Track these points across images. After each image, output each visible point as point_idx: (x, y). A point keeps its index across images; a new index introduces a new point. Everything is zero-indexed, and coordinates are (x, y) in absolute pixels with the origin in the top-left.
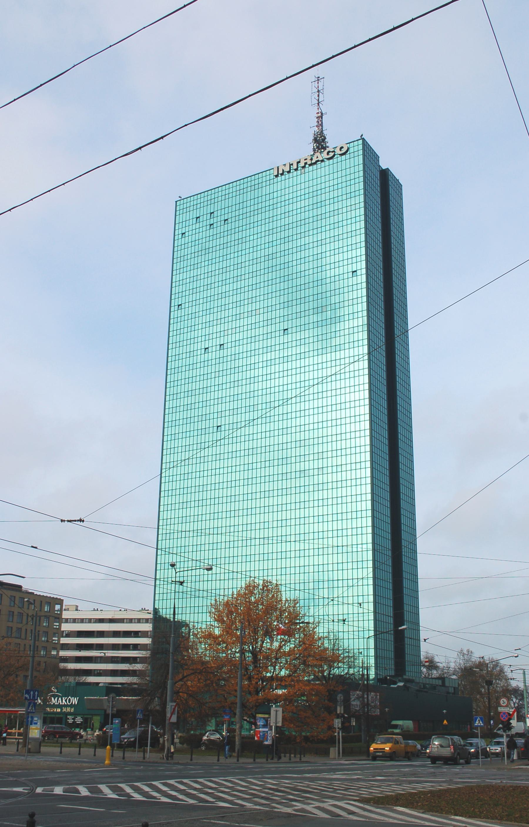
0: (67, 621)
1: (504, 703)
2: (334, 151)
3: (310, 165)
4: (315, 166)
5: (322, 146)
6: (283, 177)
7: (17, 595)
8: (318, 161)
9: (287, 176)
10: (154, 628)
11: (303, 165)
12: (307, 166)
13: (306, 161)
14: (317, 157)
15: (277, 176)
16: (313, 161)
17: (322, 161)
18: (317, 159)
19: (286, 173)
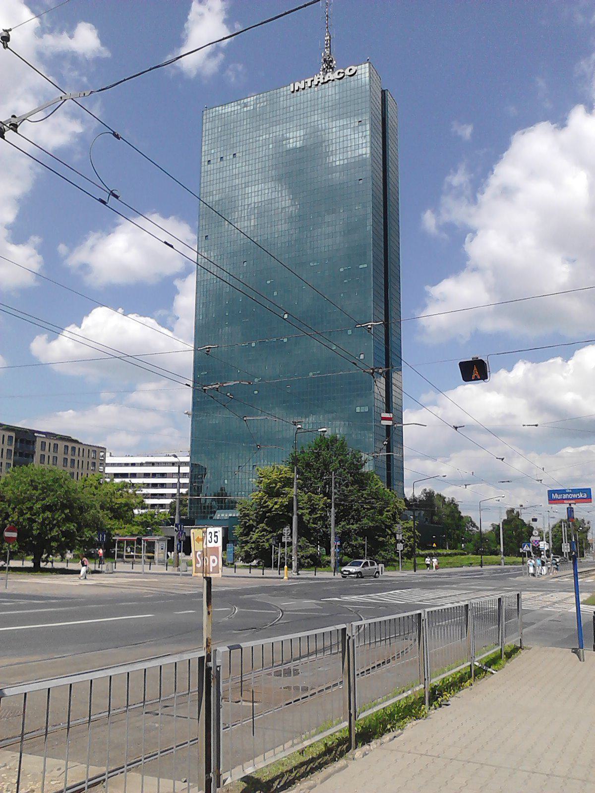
0: (108, 465)
1: (536, 533)
2: (344, 73)
4: (327, 84)
5: (330, 66)
6: (299, 93)
7: (77, 446)
8: (330, 80)
9: (302, 92)
10: (191, 471)
11: (317, 83)
12: (320, 84)
14: (329, 77)
15: (293, 92)
16: (326, 80)
17: (333, 80)
18: (329, 79)
19: (301, 90)
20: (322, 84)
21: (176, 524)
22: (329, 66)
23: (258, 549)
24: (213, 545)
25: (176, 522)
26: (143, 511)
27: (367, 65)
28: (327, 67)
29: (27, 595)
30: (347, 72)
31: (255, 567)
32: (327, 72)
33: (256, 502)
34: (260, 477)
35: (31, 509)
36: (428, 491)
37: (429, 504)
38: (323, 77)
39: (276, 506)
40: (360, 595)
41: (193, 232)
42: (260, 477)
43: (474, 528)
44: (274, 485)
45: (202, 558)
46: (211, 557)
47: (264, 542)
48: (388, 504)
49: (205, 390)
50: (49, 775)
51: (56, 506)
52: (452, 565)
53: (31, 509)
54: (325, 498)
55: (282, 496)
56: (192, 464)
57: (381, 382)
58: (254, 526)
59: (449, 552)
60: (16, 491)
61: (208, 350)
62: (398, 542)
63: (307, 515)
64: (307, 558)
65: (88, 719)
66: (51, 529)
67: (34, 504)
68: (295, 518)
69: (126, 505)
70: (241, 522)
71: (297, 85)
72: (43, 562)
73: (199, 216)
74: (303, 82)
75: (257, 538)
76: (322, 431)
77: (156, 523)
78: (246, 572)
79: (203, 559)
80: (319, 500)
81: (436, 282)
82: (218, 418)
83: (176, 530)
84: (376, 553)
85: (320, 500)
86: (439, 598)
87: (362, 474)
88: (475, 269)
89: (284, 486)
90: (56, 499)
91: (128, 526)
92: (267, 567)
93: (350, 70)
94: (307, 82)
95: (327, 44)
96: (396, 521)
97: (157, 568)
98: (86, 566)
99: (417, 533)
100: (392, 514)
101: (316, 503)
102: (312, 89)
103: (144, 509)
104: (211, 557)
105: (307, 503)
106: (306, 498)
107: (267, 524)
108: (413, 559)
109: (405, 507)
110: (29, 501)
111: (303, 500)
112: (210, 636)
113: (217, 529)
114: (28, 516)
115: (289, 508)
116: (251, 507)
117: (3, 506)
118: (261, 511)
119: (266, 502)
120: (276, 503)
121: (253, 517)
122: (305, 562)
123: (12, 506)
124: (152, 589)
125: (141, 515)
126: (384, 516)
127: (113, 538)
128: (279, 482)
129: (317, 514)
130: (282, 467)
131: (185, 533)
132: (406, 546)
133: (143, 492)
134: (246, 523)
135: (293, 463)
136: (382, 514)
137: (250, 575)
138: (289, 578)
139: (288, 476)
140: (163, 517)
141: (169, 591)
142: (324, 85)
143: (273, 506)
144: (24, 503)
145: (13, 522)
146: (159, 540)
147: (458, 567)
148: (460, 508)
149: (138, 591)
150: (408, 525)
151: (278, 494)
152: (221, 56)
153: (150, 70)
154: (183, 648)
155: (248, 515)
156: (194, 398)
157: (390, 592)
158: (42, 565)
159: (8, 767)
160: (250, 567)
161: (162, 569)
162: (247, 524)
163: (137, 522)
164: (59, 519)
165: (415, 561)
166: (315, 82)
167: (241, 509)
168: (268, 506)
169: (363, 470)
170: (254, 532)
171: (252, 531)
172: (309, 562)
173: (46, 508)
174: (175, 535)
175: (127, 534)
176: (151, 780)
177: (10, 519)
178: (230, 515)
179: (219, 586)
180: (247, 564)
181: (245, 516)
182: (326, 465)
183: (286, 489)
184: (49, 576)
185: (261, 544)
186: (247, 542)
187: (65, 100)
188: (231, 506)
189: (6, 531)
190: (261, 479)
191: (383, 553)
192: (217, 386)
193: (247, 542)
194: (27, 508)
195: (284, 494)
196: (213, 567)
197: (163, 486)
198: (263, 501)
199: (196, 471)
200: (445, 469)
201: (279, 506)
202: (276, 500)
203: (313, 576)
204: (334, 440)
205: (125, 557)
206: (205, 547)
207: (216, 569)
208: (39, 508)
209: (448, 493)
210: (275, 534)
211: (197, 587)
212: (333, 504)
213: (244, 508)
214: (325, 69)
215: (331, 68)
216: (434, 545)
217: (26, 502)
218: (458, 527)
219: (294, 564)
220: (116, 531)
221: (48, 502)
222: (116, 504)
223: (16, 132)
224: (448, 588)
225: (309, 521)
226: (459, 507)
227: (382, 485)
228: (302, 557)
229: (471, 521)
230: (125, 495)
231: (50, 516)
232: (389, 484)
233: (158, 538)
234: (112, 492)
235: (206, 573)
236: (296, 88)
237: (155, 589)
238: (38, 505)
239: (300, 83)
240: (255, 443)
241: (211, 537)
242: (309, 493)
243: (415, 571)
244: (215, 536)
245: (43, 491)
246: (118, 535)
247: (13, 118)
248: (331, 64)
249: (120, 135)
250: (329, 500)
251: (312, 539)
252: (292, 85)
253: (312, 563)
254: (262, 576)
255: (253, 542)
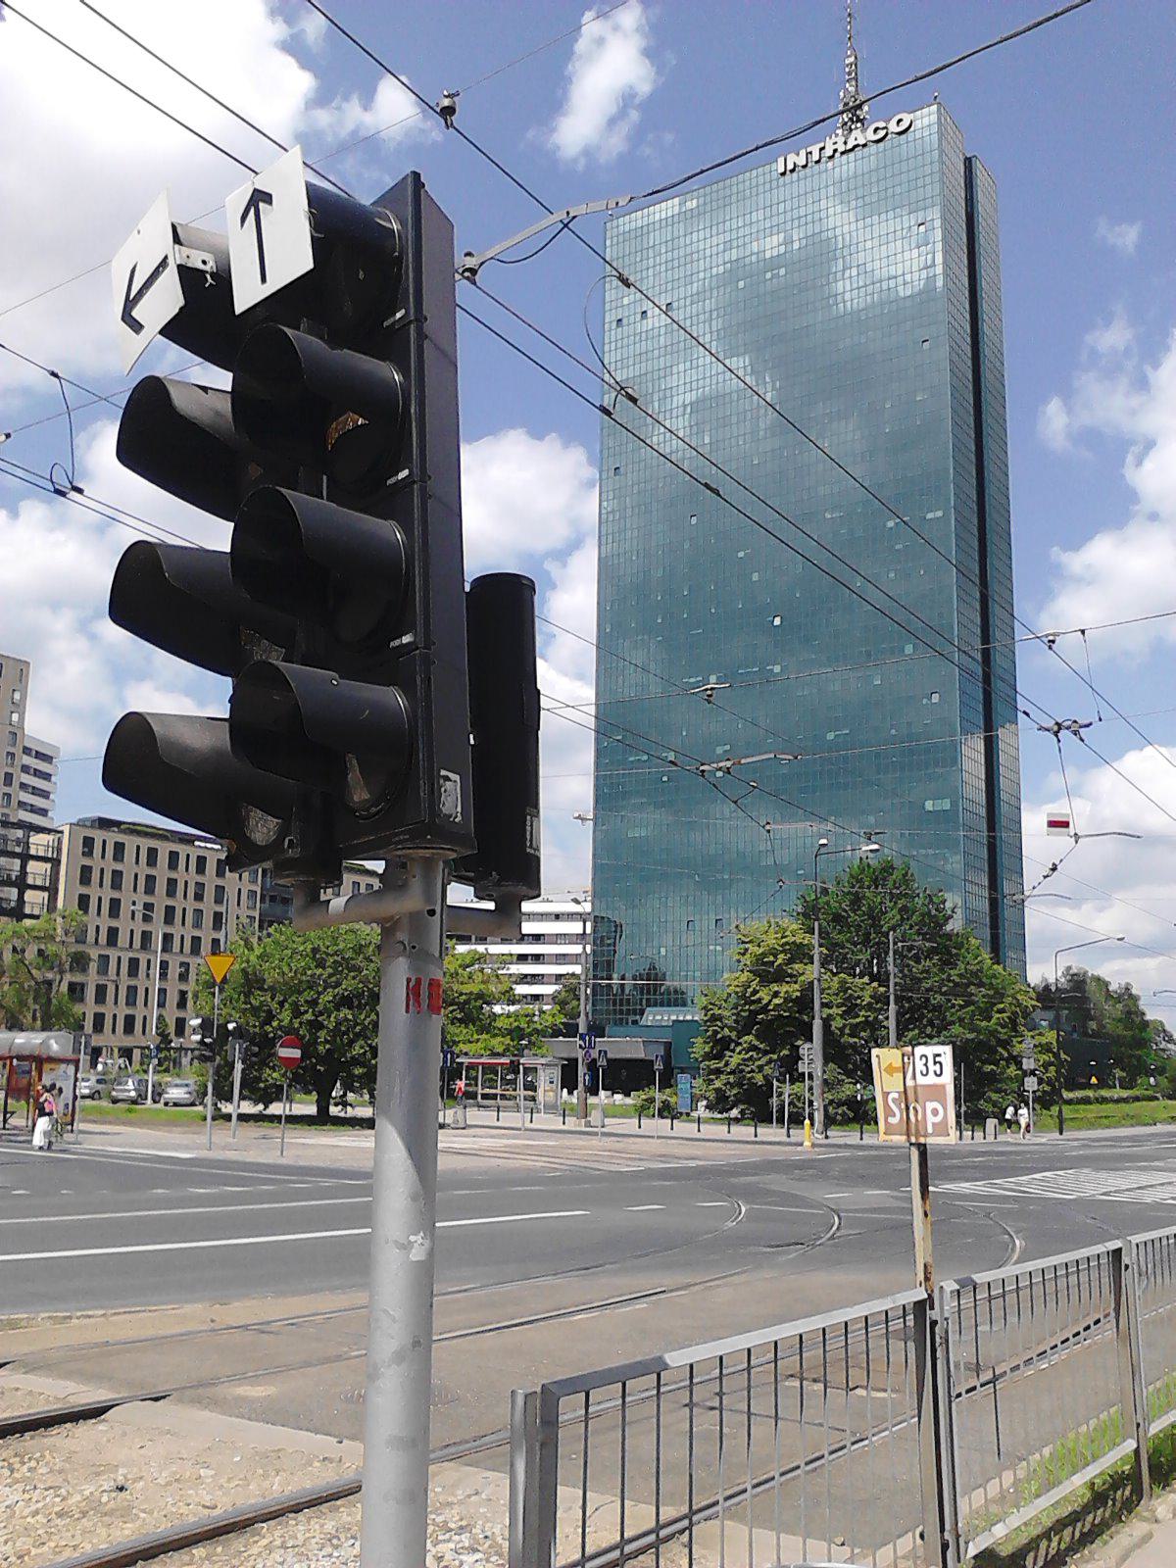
3: (842, 153)
4: (852, 155)
5: (858, 117)
6: (795, 174)
11: (831, 153)
12: (837, 155)
13: (835, 147)
15: (783, 174)
16: (849, 146)
17: (864, 145)
20: (842, 153)
21: (581, 1035)
22: (854, 113)
23: (740, 1085)
24: (931, 1079)
25: (581, 1031)
26: (512, 1008)
27: (934, 108)
28: (851, 119)
29: (331, 1170)
30: (893, 127)
31: (737, 1120)
32: (851, 130)
33: (736, 993)
34: (743, 942)
35: (313, 1003)
36: (1074, 970)
37: (1074, 999)
38: (843, 139)
39: (777, 1001)
40: (977, 1180)
41: (590, 462)
42: (743, 942)
43: (1169, 1046)
44: (772, 958)
45: (903, 1106)
46: (928, 1104)
47: (752, 1071)
48: (1002, 996)
49: (703, 771)
50: (565, 1515)
51: (361, 995)
52: (1136, 1120)
53: (313, 1003)
54: (875, 984)
55: (788, 979)
56: (596, 917)
57: (973, 751)
58: (733, 1041)
59: (1125, 1094)
60: (286, 969)
61: (709, 692)
62: (1025, 1074)
63: (838, 1018)
64: (840, 1104)
65: (583, 1412)
66: (351, 1042)
67: (319, 993)
68: (817, 1025)
69: (480, 996)
70: (707, 1031)
71: (792, 159)
72: (336, 1105)
73: (602, 430)
74: (803, 153)
75: (739, 1064)
76: (871, 851)
77: (537, 1031)
78: (721, 1131)
79: (907, 1108)
80: (862, 989)
81: (1077, 541)
82: (644, 824)
83: (580, 1046)
84: (981, 1096)
85: (864, 989)
86: (1139, 1188)
87: (949, 936)
88: (1154, 517)
89: (791, 961)
90: (361, 985)
91: (484, 1036)
92: (763, 1121)
93: (900, 121)
94: (811, 153)
95: (849, 74)
96: (1016, 1031)
97: (543, 1121)
98: (50, 1114)
99: (1063, 1056)
100: (1009, 1018)
101: (856, 995)
102: (822, 166)
103: (513, 1004)
104: (928, 1104)
105: (837, 995)
106: (835, 984)
107: (757, 1037)
108: (1055, 1109)
109: (1034, 1003)
110: (311, 988)
111: (829, 988)
112: (930, 1260)
113: (939, 1049)
114: (309, 1016)
115: (804, 1002)
116: (725, 1001)
117: (262, 999)
118: (745, 1011)
119: (755, 992)
120: (776, 994)
121: (730, 1022)
122: (837, 1113)
123: (279, 998)
124: (557, 1160)
125: (508, 1016)
126: (993, 1021)
127: (458, 1060)
128: (782, 952)
129: (858, 1016)
130: (785, 922)
131: (605, 1052)
132: (1040, 1081)
133: (510, 972)
134: (716, 1033)
135: (805, 915)
136: (989, 1019)
137: (729, 1137)
138: (814, 1145)
139: (798, 941)
140: (550, 1019)
141: (586, 1164)
142: (845, 157)
143: (770, 1001)
144: (300, 993)
145: (280, 1027)
146: (546, 1065)
147: (1145, 1125)
148: (1142, 1005)
149: (529, 1163)
150: (1044, 1040)
151: (780, 976)
152: (634, 115)
153: (757, 149)
154: (667, 1280)
155: (720, 1018)
156: (597, 787)
157: (1035, 1176)
158: (334, 1110)
159: (484, 1496)
160: (730, 1121)
161: (556, 1122)
162: (719, 1036)
163: (500, 1029)
164: (366, 1023)
165: (1060, 1111)
166: (829, 152)
167: (705, 1008)
168: (760, 1000)
169: (948, 928)
170: (733, 1051)
171: (728, 1049)
172: (844, 1114)
173: (345, 1001)
174: (580, 1054)
175: (483, 1052)
176: (765, 1537)
177: (275, 1024)
178: (674, 1018)
179: (680, 1158)
180: (719, 1116)
181: (717, 1020)
182: (874, 917)
183: (796, 966)
184: (349, 1133)
185: (749, 1075)
186: (718, 1072)
187: (574, 217)
188: (677, 999)
189: (281, 1046)
190: (747, 946)
191: (995, 1096)
192: (728, 764)
193: (718, 1072)
194: (306, 1001)
195: (791, 976)
196: (934, 1124)
197: (537, 958)
198: (750, 990)
199: (603, 931)
200: (1105, 922)
201: (782, 1001)
202: (776, 989)
203: (785, 1139)
204: (888, 868)
205: (479, 1097)
206: (910, 1083)
207: (941, 1129)
208: (329, 1002)
209: (1114, 972)
210: (775, 1057)
211: (640, 1160)
212: (892, 998)
213: (711, 1004)
214: (846, 124)
215: (859, 120)
216: (1094, 1080)
217: (305, 990)
218: (1142, 1043)
219: (818, 1117)
220: (461, 1045)
221: (346, 990)
222: (461, 994)
223: (474, 283)
224: (1144, 1169)
225: (842, 1030)
226: (1141, 1003)
227: (986, 955)
228: (831, 1102)
229: (1164, 1031)
230: (478, 977)
231: (350, 1017)
232: (997, 958)
233: (543, 1061)
234: (452, 971)
235: (918, 1135)
236: (790, 166)
237: (562, 1161)
238: (326, 998)
239: (798, 154)
240: (714, 875)
241: (926, 1065)
242: (842, 975)
243: (1061, 1133)
244: (935, 1063)
245: (335, 969)
246: (466, 1054)
247: (468, 258)
248: (858, 112)
249: (632, 279)
250: (882, 989)
251: (851, 1066)
252: (781, 160)
253: (851, 1115)
254: (753, 1139)
255: (732, 1072)
